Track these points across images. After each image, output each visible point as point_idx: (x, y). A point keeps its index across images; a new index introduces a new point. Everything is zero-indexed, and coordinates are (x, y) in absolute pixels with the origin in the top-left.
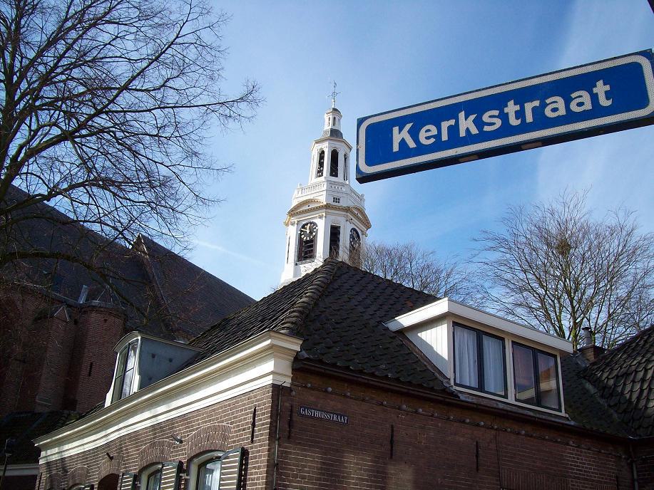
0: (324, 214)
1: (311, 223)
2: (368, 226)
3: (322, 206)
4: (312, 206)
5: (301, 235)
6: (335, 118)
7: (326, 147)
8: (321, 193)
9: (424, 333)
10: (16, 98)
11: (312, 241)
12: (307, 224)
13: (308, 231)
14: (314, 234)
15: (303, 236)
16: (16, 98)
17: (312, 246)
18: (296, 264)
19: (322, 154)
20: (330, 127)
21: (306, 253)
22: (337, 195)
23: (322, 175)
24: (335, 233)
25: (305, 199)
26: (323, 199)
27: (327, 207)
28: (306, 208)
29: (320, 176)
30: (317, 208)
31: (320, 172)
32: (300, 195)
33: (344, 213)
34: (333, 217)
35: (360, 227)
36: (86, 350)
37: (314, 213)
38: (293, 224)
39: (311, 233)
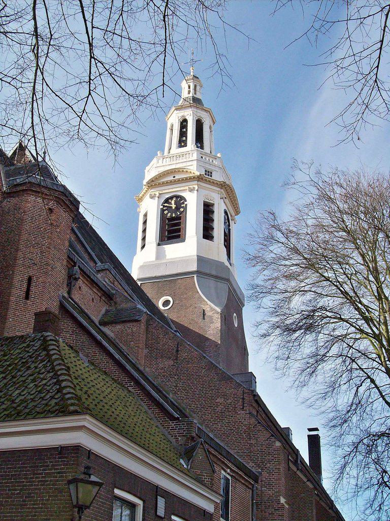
0: (196, 187)
1: (177, 197)
2: (237, 213)
3: (194, 177)
4: (178, 177)
5: (163, 211)
6: (195, 86)
7: (190, 115)
8: (190, 163)
9: (7, 153)
10: (307, 460)
11: (179, 218)
12: (171, 198)
13: (174, 206)
14: (182, 210)
15: (166, 212)
16: (307, 460)
17: (179, 224)
18: (159, 245)
19: (184, 124)
20: (191, 95)
21: (170, 232)
22: (209, 168)
23: (185, 145)
24: (208, 210)
25: (173, 167)
26: (194, 169)
27: (199, 178)
28: (171, 178)
29: (183, 147)
30: (186, 179)
31: (182, 142)
32: (160, 163)
33: (218, 189)
34: (206, 192)
35: (231, 211)
36: (20, 254)
37: (184, 184)
38: (152, 197)
39: (177, 208)
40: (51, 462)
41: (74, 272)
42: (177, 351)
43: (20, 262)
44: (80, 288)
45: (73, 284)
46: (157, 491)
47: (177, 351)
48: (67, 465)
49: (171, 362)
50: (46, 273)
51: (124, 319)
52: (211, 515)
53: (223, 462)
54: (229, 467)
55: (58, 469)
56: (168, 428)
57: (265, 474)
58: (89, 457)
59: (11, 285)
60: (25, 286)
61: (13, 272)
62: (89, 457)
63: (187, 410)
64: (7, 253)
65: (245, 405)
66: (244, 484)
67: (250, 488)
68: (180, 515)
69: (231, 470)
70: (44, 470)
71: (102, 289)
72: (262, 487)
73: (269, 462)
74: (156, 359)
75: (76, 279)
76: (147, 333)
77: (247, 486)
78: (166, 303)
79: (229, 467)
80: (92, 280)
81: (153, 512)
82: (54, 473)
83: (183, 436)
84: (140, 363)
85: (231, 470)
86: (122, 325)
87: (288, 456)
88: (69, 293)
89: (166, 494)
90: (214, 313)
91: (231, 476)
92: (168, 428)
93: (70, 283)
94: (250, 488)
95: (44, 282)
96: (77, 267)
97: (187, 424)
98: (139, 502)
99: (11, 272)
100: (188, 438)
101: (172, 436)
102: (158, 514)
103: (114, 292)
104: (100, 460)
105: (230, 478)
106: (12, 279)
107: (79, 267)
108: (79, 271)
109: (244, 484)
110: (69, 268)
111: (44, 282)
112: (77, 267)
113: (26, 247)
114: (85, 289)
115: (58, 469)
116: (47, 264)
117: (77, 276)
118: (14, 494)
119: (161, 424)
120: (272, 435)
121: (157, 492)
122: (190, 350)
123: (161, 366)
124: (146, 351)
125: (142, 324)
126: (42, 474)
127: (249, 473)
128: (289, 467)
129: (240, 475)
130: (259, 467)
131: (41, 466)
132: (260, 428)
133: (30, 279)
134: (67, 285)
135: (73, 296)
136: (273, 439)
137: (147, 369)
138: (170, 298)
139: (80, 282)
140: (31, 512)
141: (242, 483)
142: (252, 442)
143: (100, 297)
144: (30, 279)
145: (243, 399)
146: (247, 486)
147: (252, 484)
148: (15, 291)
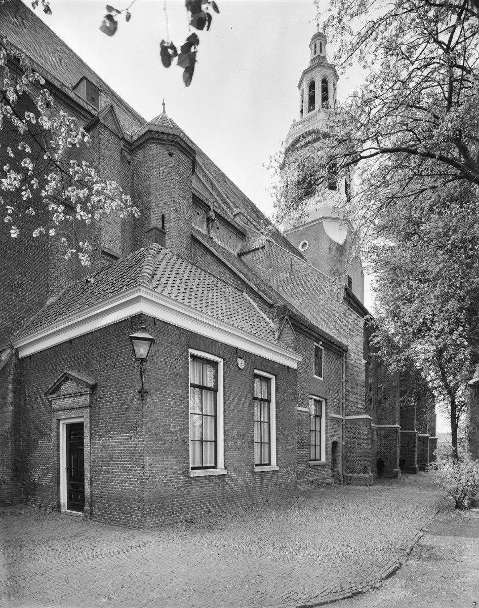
43: (153, 204)
45: (211, 225)
52: (296, 370)
71: (236, 228)
78: (305, 245)
126: (122, 341)
133: (163, 217)
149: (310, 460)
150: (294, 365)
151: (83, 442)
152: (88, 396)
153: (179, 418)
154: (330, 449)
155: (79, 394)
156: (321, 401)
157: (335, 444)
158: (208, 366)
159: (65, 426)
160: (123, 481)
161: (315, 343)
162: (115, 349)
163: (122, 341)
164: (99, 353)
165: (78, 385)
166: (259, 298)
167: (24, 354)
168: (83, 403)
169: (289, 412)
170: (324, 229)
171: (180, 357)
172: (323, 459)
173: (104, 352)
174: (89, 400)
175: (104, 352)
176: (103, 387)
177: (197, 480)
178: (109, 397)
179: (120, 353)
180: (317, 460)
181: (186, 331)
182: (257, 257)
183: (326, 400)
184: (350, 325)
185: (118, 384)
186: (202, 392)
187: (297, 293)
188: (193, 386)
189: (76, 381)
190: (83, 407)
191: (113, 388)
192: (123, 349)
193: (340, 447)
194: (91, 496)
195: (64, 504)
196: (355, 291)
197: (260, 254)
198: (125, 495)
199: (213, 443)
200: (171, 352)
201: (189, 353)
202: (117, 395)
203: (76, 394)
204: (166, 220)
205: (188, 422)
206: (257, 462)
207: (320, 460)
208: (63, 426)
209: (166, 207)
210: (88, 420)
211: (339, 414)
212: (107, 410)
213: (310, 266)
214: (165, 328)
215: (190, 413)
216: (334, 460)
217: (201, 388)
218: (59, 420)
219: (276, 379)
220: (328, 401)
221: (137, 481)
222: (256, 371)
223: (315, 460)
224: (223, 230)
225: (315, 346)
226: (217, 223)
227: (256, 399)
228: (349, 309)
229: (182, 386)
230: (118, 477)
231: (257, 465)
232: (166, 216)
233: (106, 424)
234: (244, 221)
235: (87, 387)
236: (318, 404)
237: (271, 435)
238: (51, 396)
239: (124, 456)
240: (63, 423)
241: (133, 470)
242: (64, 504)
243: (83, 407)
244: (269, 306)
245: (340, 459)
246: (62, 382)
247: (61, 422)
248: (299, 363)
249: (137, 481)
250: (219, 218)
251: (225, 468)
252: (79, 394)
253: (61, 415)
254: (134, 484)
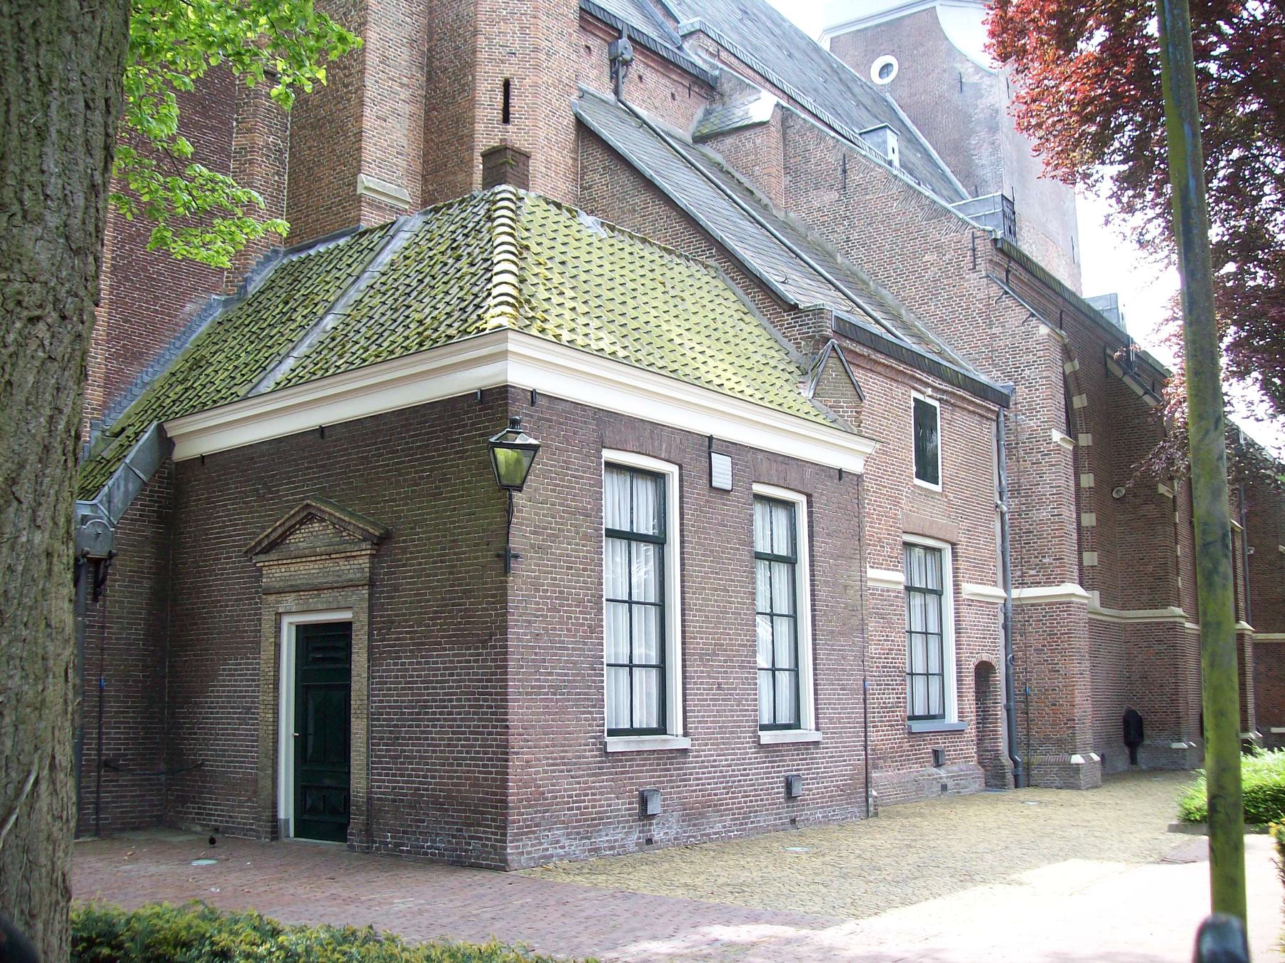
40: (470, 418)
41: (620, 51)
42: (845, 171)
43: (482, 56)
44: (640, 78)
45: (621, 74)
46: (710, 444)
47: (845, 171)
48: (492, 420)
49: (834, 195)
50: (536, 67)
51: (739, 124)
52: (859, 476)
53: (913, 377)
54: (927, 385)
55: (479, 429)
56: (781, 325)
57: (1021, 390)
58: (533, 403)
59: (472, 102)
60: (500, 98)
61: (474, 77)
62: (533, 403)
63: (871, 283)
64: (459, 42)
65: (979, 261)
66: (974, 412)
67: (992, 419)
68: (775, 481)
69: (934, 388)
70: (460, 433)
71: (689, 73)
72: (1016, 415)
73: (1028, 366)
74: (806, 191)
75: (627, 63)
76: (785, 145)
77: (981, 416)
78: (886, 69)
79: (927, 385)
80: (662, 57)
81: (705, 481)
82: (475, 436)
83: (809, 337)
84: (775, 205)
85: (934, 388)
86: (734, 137)
87: (1105, 349)
88: (616, 92)
89: (731, 448)
90: (982, 77)
91: (940, 400)
92: (781, 325)
93: (617, 73)
94: (992, 419)
95: (536, 85)
96: (625, 39)
97: (814, 315)
98: (672, 470)
99: (470, 77)
100: (819, 341)
101: (790, 340)
102: (714, 484)
103: (717, 73)
104: (564, 404)
105: (936, 404)
106: (474, 89)
107: (630, 37)
108: (629, 45)
109: (974, 412)
110: (609, 44)
111: (536, 85)
112: (625, 39)
113: (492, 24)
114: (652, 78)
115: (479, 429)
116: (536, 50)
117: (627, 57)
118: (421, 478)
119: (769, 319)
120: (1033, 315)
121: (710, 447)
122: (867, 167)
123: (816, 204)
124: (785, 180)
125: (772, 129)
126: (458, 440)
127: (982, 391)
128: (1107, 370)
129: (961, 396)
130: (1010, 377)
131: (457, 428)
132: (1009, 302)
133: (507, 85)
134: (612, 78)
135: (623, 98)
136: (1034, 321)
137: (792, 215)
138: (889, 59)
139: (638, 67)
140: (449, 504)
141: (969, 411)
142: (994, 330)
143: (689, 89)
144: (507, 85)
145: (974, 250)
146: (981, 416)
147: (994, 411)
148: (480, 113)
149: (913, 718)
150: (854, 465)
151: (350, 670)
152: (367, 561)
153: (581, 612)
154: (970, 681)
155: (343, 555)
156: (940, 550)
157: (984, 671)
158: (640, 482)
159: (294, 628)
160: (455, 759)
161: (914, 394)
162: (440, 456)
163: (458, 440)
164: (398, 463)
165: (338, 533)
166: (759, 286)
167: (184, 452)
168: (351, 576)
169: (846, 587)
170: (941, 30)
171: (584, 472)
172: (952, 718)
173: (410, 461)
174: (367, 570)
175: (410, 461)
176: (404, 541)
177: (621, 761)
178: (420, 564)
179: (452, 466)
180: (934, 717)
181: (598, 411)
182: (749, 145)
183: (953, 545)
184: (1013, 336)
185: (445, 536)
186: (629, 546)
187: (863, 245)
188: (612, 534)
189: (334, 524)
190: (352, 585)
191: (431, 544)
192: (461, 458)
193: (1000, 675)
194: (370, 799)
195: (287, 821)
196: (1029, 245)
197: (758, 138)
198: (459, 791)
199: (654, 673)
200: (565, 462)
201: (603, 461)
202: (442, 562)
203: (333, 556)
204: (514, 92)
205: (601, 620)
206: (766, 719)
207: (943, 716)
208: (289, 630)
209: (513, 60)
210: (364, 617)
211: (995, 583)
212: (415, 595)
213: (896, 177)
214: (552, 409)
215: (604, 599)
216: (984, 716)
217: (630, 537)
218: (279, 615)
219: (810, 504)
220: (960, 550)
221: (491, 759)
222: (759, 488)
223: (929, 717)
224: (654, 79)
225: (915, 399)
226: (638, 67)
227: (759, 556)
228: (1006, 293)
229: (586, 537)
230: (441, 752)
231: (764, 728)
232: (515, 83)
233: (410, 626)
234: (711, 49)
235: (364, 540)
236: (929, 557)
237: (702, 219)
238: (262, 557)
239: (458, 700)
240: (291, 623)
241: (482, 733)
242: (287, 821)
243: (352, 585)
244: (787, 309)
245: (1002, 714)
246: (295, 525)
247: (286, 621)
248: (868, 459)
249: (491, 759)
250: (642, 54)
251: (685, 734)
252: (343, 555)
253: (290, 601)
254: (484, 766)
